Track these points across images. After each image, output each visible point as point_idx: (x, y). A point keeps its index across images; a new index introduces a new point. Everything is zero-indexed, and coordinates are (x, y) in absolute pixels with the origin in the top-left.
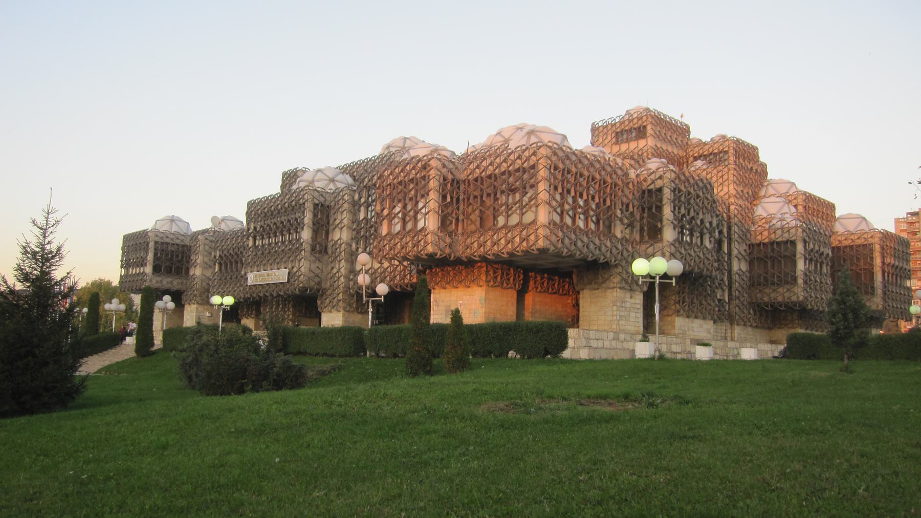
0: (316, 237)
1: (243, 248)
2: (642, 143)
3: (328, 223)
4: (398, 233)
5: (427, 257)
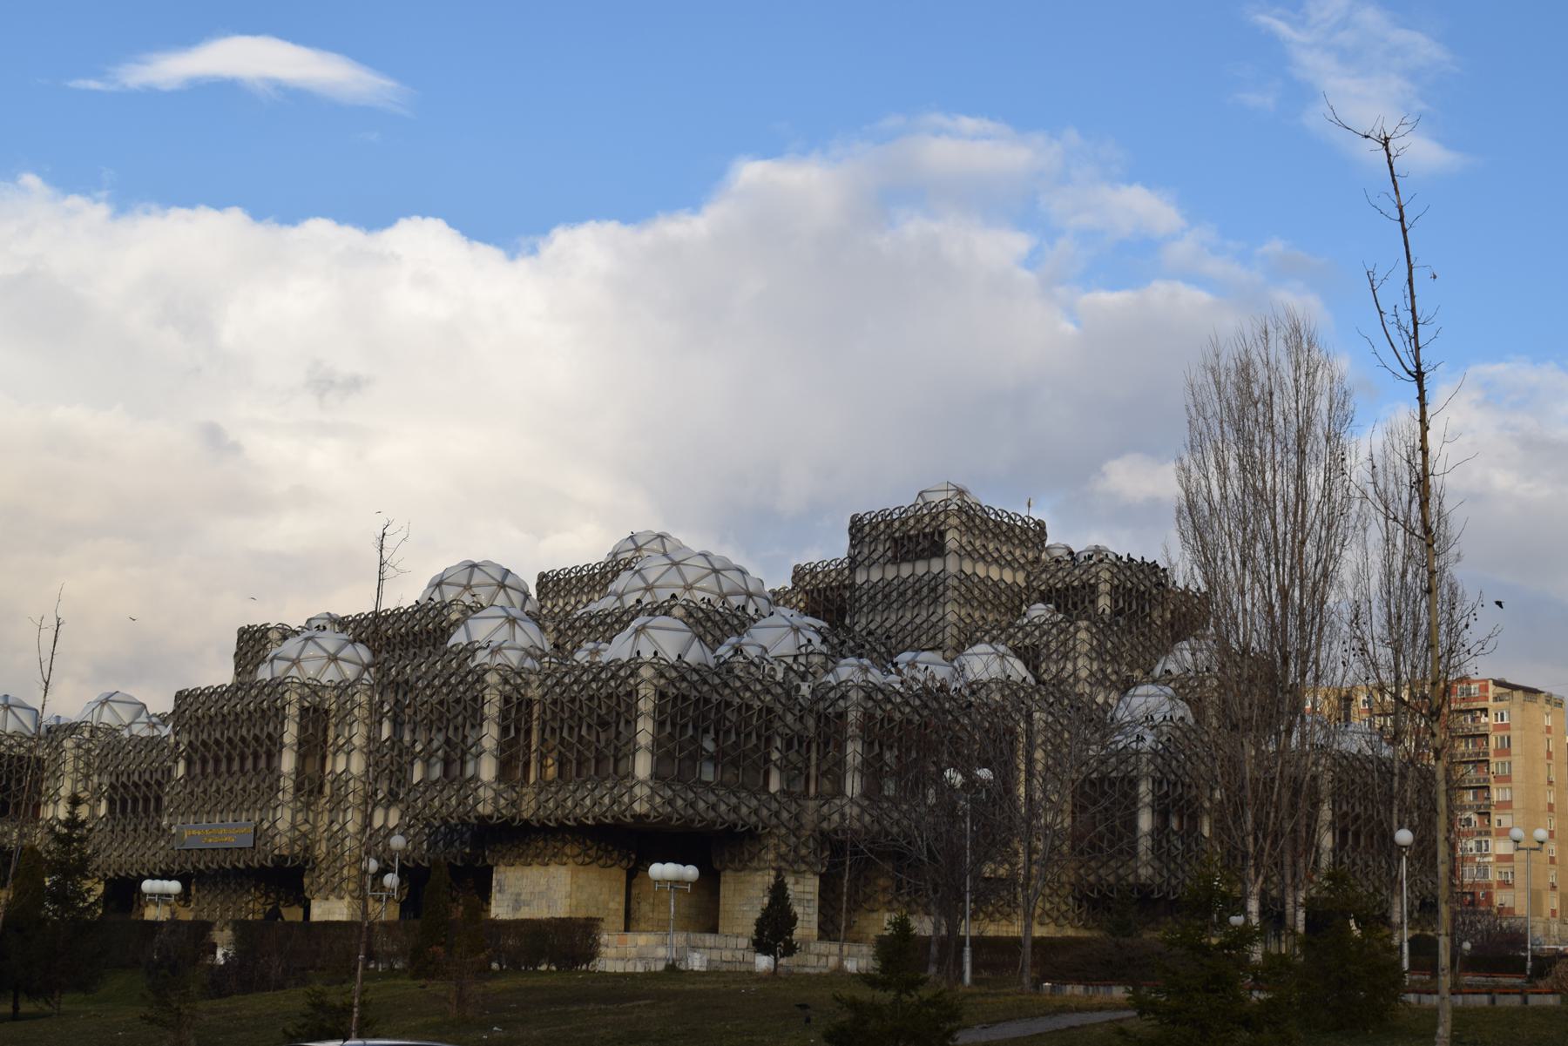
0: (303, 766)
1: (160, 772)
2: (936, 565)
3: (325, 741)
4: (437, 781)
5: (476, 822)
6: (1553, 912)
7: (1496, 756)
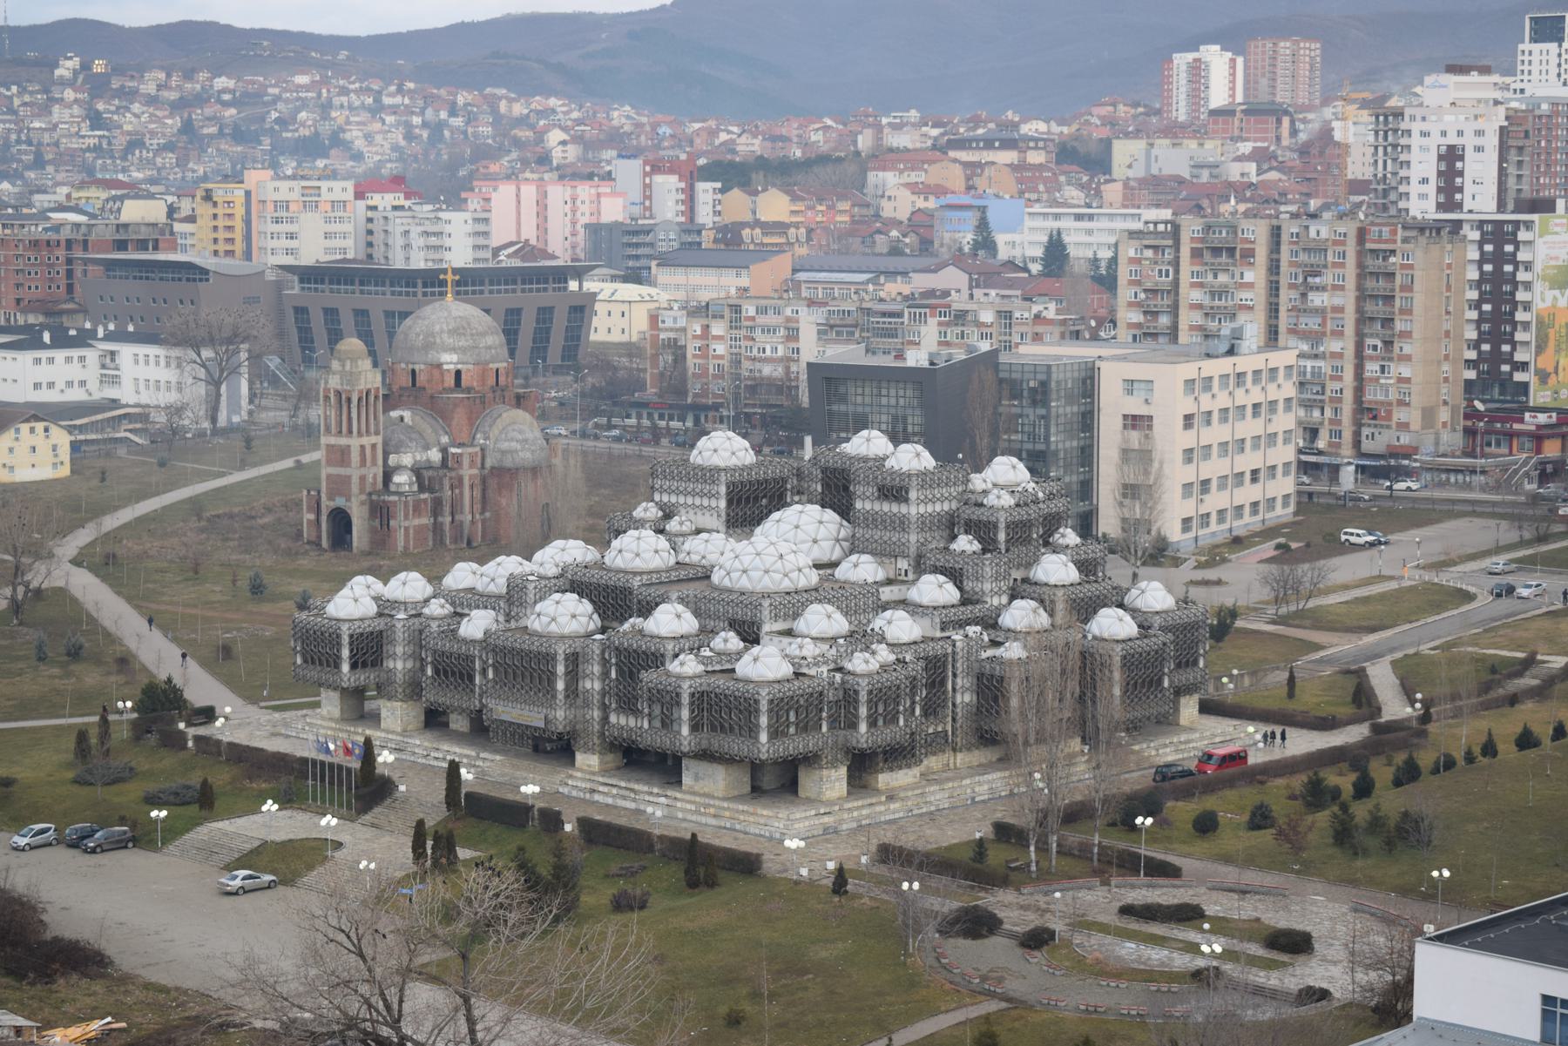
2: (904, 509)
6: (1444, 424)
7: (1401, 291)
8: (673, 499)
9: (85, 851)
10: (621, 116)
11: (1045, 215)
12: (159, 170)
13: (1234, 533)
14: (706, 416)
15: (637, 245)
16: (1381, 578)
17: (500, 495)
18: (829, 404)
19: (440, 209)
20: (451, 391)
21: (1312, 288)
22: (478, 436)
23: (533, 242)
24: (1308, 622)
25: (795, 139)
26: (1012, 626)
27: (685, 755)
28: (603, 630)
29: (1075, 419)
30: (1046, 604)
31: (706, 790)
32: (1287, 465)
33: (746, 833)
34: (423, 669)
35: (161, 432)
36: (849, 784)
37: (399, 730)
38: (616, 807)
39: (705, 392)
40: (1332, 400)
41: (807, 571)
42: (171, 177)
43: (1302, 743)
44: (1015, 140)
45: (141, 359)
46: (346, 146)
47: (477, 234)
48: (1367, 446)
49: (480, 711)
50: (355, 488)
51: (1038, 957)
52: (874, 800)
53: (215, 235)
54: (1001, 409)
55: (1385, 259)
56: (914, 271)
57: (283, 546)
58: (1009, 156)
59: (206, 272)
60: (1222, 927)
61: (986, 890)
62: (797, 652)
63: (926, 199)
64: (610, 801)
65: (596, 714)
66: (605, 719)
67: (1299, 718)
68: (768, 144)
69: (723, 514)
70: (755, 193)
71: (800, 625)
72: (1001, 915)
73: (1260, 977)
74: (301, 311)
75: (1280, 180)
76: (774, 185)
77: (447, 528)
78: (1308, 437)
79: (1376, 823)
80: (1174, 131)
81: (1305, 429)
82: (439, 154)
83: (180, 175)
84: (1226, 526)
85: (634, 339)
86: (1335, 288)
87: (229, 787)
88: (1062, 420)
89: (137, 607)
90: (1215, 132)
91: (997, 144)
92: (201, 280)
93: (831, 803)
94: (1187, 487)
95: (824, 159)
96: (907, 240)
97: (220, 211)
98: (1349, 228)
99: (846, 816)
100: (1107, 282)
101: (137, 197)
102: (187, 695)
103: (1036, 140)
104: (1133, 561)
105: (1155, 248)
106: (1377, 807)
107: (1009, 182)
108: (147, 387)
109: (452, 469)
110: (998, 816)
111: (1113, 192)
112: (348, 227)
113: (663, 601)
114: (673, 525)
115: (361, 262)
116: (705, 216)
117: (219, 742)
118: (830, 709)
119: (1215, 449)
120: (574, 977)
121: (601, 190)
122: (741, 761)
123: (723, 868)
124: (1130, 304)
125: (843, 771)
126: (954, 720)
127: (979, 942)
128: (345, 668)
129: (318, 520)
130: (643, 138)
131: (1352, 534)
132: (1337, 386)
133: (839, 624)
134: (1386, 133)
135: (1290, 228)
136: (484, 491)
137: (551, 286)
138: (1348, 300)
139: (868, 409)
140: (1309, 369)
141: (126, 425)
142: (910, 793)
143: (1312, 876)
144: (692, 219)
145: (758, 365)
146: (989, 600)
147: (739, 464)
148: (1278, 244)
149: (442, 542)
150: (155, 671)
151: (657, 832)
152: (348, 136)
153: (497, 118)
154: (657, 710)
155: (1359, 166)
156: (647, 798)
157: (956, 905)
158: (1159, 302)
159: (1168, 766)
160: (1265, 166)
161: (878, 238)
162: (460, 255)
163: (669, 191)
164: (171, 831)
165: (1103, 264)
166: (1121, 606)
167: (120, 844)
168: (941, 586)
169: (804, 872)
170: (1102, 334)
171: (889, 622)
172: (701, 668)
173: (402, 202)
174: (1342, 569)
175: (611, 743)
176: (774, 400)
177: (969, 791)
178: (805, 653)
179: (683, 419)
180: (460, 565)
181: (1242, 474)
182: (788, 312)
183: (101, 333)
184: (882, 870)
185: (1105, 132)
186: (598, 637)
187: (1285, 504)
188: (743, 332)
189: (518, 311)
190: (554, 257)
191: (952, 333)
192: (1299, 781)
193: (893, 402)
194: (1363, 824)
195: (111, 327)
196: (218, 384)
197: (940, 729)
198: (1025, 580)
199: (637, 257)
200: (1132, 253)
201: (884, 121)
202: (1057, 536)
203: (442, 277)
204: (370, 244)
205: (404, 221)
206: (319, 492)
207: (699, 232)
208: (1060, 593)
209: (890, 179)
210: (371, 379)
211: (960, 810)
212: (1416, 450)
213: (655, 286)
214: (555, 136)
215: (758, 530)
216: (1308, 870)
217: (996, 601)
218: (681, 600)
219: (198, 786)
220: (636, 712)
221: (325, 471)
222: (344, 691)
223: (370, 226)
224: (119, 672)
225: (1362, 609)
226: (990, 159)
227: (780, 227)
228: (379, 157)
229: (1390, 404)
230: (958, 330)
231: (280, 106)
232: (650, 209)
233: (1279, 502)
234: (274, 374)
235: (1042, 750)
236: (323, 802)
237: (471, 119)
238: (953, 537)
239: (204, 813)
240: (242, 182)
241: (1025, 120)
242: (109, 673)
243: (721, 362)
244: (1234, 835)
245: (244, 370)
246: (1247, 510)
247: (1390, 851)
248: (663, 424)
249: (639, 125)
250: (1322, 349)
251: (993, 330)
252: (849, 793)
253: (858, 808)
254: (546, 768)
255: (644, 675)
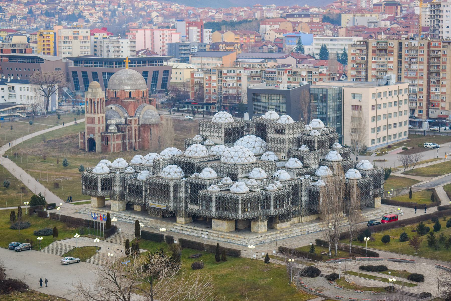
2: (284, 136)
8: (207, 134)
9: (16, 251)
10: (175, 7)
11: (320, 39)
12: (21, 26)
13: (388, 144)
14: (211, 107)
15: (185, 50)
16: (438, 159)
17: (144, 133)
18: (254, 102)
19: (119, 38)
20: (128, 99)
21: (412, 63)
22: (137, 113)
23: (150, 49)
24: (414, 174)
25: (234, 14)
26: (320, 175)
27: (214, 218)
28: (185, 177)
29: (336, 107)
30: (332, 168)
31: (221, 229)
32: (405, 122)
33: (234, 244)
34: (125, 190)
35: (29, 113)
36: (267, 227)
37: (117, 210)
38: (191, 235)
39: (210, 99)
40: (419, 100)
41: (252, 157)
42: (25, 28)
43: (421, 213)
44: (309, 14)
45: (22, 89)
46: (84, 17)
47: (131, 47)
48: (431, 115)
49: (145, 204)
50: (97, 131)
51: (334, 283)
52: (276, 232)
53: (44, 48)
54: (311, 104)
55: (437, 53)
56: (278, 58)
57: (73, 150)
58: (306, 20)
59: (43, 60)
60: (394, 273)
61: (315, 262)
62: (250, 184)
63: (280, 34)
64: (188, 233)
65: (184, 204)
66: (186, 207)
67: (414, 205)
68: (225, 16)
69: (223, 138)
70: (223, 32)
71: (251, 175)
72: (320, 270)
73: (406, 289)
74: (75, 73)
75: (398, 27)
76: (229, 30)
77: (127, 144)
78: (411, 112)
79: (442, 239)
80: (361, 11)
81: (410, 110)
82: (115, 20)
83: (28, 28)
84: (386, 142)
85: (185, 81)
86: (420, 63)
87: (62, 230)
88: (331, 107)
89: (26, 171)
90: (375, 11)
91: (303, 16)
92: (41, 62)
93: (262, 233)
94: (373, 129)
95: (245, 21)
96: (274, 48)
97: (45, 39)
98: (425, 43)
99: (267, 238)
100: (343, 60)
101: (17, 35)
102: (46, 200)
103: (316, 14)
104: (356, 153)
105: (360, 50)
106: (443, 234)
107: (308, 28)
108: (25, 98)
109: (128, 125)
110: (317, 237)
111: (342, 31)
112: (89, 45)
113: (205, 167)
114: (207, 142)
115: (93, 56)
116: (206, 40)
117: (58, 215)
118: (261, 202)
119: (382, 116)
120: (187, 289)
121: (172, 32)
122: (232, 220)
123: (228, 255)
124: (352, 69)
125: (266, 223)
126: (301, 206)
127: (314, 278)
128: (100, 190)
129: (84, 142)
130: (184, 14)
131: (428, 144)
132: (421, 95)
133: (264, 175)
134: (434, 11)
135: (405, 43)
136: (139, 132)
137: (158, 64)
138: (424, 67)
139: (267, 104)
140: (412, 90)
141: (18, 111)
142: (287, 230)
143: (422, 256)
144: (202, 41)
145: (228, 90)
146: (312, 166)
147: (228, 122)
148: (401, 48)
149: (125, 149)
150: (34, 191)
151: (205, 243)
152: (84, 14)
153: (134, 8)
154: (204, 203)
155: (425, 21)
156: (201, 232)
157: (305, 266)
158: (362, 68)
159: (372, 221)
160: (393, 23)
161: (264, 47)
162: (126, 54)
163: (195, 32)
164: (44, 244)
165: (340, 56)
166: (355, 168)
167: (27, 249)
168: (296, 162)
169: (255, 256)
170: (341, 79)
171: (280, 174)
172: (219, 189)
173: (106, 36)
174: (425, 156)
175: (189, 214)
176: (233, 101)
177: (307, 229)
178: (253, 184)
179: (203, 108)
180: (136, 156)
181: (391, 124)
182: (238, 72)
183: (9, 80)
184: (280, 255)
185: (338, 11)
186: (184, 179)
187: (405, 135)
188: (223, 79)
189: (157, 72)
190: (157, 54)
191: (292, 79)
192: (416, 226)
193: (275, 101)
194: (438, 239)
195: (12, 78)
196: (48, 97)
197: (297, 209)
198: (324, 160)
199: (184, 54)
200: (352, 52)
201: (264, 8)
202: (334, 145)
203: (124, 61)
204: (96, 50)
205: (107, 42)
206: (84, 132)
207: (205, 46)
208: (336, 164)
209: (268, 27)
210: (101, 94)
211: (304, 235)
212: (447, 116)
213: (191, 63)
214: (154, 14)
215: (235, 144)
216: (420, 255)
217: (314, 167)
218: (211, 167)
219: (52, 229)
220: (197, 204)
221: (87, 125)
222: (99, 198)
223: (96, 44)
224: (23, 192)
225: (433, 169)
226: (301, 21)
227: (232, 44)
228: (94, 21)
229: (439, 101)
230: (294, 77)
231: (61, 4)
232: (188, 38)
233: (403, 134)
234: (66, 94)
235: (331, 216)
236: (94, 234)
237: (125, 8)
238: (300, 146)
239: (54, 238)
240: (53, 30)
241: (311, 7)
242: (18, 193)
243: (215, 89)
244: (395, 243)
245: (57, 92)
246: (392, 137)
247: (447, 248)
248: (196, 109)
249: (182, 10)
250: (416, 83)
251: (306, 78)
252: (268, 230)
253: (270, 235)
254: (167, 222)
255: (200, 192)
